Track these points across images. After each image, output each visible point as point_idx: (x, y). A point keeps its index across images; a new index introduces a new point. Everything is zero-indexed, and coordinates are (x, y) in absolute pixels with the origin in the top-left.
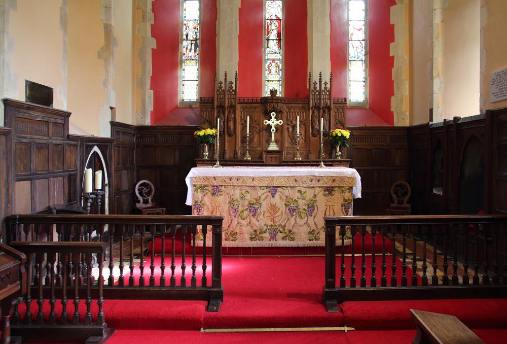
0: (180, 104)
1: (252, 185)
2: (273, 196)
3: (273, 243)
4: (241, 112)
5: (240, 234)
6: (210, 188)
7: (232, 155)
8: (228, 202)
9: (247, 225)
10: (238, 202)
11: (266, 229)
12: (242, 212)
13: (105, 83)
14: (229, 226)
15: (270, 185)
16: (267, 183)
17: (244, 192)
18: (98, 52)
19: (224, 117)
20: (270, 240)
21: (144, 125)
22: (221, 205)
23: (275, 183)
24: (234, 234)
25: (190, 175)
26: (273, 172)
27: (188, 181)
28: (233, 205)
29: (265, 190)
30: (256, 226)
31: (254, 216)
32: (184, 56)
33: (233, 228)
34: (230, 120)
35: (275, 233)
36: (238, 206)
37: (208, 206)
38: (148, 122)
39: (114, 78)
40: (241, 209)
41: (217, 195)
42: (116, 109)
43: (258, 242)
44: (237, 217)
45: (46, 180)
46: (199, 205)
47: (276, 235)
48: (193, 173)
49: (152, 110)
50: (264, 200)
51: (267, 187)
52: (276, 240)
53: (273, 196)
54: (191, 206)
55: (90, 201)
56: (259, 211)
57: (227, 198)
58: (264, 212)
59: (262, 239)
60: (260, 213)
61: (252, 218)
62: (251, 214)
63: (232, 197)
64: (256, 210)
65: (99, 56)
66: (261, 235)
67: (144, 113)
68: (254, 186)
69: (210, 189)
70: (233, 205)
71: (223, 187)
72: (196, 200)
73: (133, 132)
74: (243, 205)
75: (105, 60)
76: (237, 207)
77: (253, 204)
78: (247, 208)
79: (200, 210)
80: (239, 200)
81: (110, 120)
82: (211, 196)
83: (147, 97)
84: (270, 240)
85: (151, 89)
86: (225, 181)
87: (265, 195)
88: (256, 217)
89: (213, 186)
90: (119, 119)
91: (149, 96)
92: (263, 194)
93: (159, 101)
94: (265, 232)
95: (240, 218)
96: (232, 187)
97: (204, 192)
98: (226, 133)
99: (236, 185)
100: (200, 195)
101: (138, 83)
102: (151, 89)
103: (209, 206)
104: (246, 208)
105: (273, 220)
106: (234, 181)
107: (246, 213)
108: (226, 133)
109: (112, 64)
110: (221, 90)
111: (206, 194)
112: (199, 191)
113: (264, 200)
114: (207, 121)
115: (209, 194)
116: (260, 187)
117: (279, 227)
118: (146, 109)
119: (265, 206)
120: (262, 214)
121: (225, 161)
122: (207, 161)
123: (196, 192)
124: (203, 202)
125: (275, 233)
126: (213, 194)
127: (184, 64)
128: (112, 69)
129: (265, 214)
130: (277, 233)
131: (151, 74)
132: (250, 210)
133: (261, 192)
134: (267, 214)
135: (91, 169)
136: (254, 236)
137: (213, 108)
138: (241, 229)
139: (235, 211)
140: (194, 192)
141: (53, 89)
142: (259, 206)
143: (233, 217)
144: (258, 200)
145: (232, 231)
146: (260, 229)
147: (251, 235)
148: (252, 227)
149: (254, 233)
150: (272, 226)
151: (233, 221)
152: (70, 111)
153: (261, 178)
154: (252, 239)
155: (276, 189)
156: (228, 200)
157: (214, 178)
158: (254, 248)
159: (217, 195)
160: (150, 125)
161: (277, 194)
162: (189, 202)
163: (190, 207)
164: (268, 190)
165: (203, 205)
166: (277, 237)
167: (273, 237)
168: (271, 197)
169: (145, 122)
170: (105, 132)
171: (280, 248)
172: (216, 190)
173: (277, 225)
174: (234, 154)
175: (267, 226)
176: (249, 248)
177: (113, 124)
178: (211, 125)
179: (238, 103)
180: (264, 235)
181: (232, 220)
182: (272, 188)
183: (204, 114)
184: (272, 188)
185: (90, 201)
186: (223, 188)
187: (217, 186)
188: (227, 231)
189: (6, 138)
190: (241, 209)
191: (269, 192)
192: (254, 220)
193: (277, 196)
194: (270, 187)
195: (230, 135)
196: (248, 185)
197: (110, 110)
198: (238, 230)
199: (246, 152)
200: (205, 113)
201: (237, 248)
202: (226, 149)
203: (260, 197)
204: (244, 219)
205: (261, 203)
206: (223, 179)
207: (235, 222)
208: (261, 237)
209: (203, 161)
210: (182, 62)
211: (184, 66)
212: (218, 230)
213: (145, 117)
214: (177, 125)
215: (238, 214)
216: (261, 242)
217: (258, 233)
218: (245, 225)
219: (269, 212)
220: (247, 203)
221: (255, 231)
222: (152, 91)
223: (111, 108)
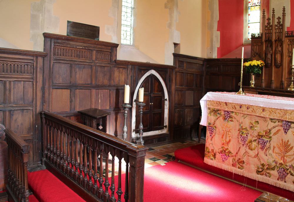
0: (245, 42)
1: (262, 115)
2: (286, 132)
3: (281, 184)
4: (289, 45)
5: (247, 164)
6: (223, 113)
7: (278, 85)
8: (237, 129)
9: (255, 157)
10: (247, 130)
11: (275, 167)
12: (251, 142)
13: (170, 26)
14: (237, 153)
15: (282, 119)
16: (278, 115)
17: (254, 122)
18: (165, 4)
19: (272, 49)
20: (278, 179)
21: (212, 58)
22: (231, 131)
23: (288, 118)
24: (241, 162)
25: (205, 98)
26: (286, 105)
27: (203, 102)
28: (242, 133)
29: (277, 123)
30: (264, 160)
31: (262, 148)
32: (250, 4)
33: (240, 156)
34: (277, 53)
35: (284, 173)
36: (247, 135)
37: (219, 130)
38: (215, 56)
39: (178, 22)
40: (249, 138)
41: (228, 121)
42: (181, 44)
43: (264, 177)
44: (245, 146)
45: (90, 91)
46: (212, 127)
47: (286, 176)
48: (208, 96)
49: (219, 46)
50: (275, 134)
51: (279, 121)
52: (285, 182)
53: (286, 132)
54: (206, 126)
55: (127, 109)
56: (268, 144)
57: (237, 125)
58: (274, 147)
59: (270, 176)
60: (269, 147)
61: (260, 150)
62: (260, 146)
63: (241, 125)
64: (265, 143)
65: (166, 7)
66: (268, 171)
67: (212, 48)
68: (264, 118)
69: (222, 114)
70: (242, 133)
71: (234, 113)
72: (209, 122)
73: (201, 63)
74: (252, 136)
75: (170, 9)
76: (245, 136)
77: (262, 136)
78: (256, 138)
79: (212, 131)
80: (248, 129)
81: (173, 52)
82: (223, 120)
83: (214, 37)
84: (278, 179)
85: (218, 30)
86: (235, 108)
87: (277, 128)
88: (264, 150)
89: (225, 111)
90: (183, 52)
91: (216, 36)
92: (274, 127)
93: (224, 39)
94: (273, 169)
95: (248, 147)
96: (242, 115)
97: (217, 116)
98: (273, 64)
99: (246, 113)
100: (213, 118)
101: (206, 26)
102: (218, 30)
103: (221, 130)
104: (254, 139)
105: (283, 157)
106: (244, 108)
107: (254, 144)
108: (273, 64)
109: (175, 12)
110: (269, 26)
111: (219, 118)
112: (212, 113)
113: (275, 134)
114: (257, 54)
115: (221, 118)
116: (271, 119)
117: (290, 167)
118: (213, 46)
119: (275, 141)
120: (272, 148)
121: (261, 89)
122: (252, 88)
123: (209, 115)
124: (215, 125)
125: (284, 173)
126: (225, 119)
127: (249, 10)
128: (175, 14)
129: (275, 150)
130: (288, 174)
131: (218, 19)
132: (259, 142)
133: (271, 125)
134: (277, 150)
135: (143, 88)
136: (260, 170)
137: (262, 43)
138: (248, 159)
139: (244, 140)
140: (209, 114)
141: (99, 27)
142: (269, 140)
143: (241, 145)
144: (268, 132)
145: (240, 159)
146: (268, 165)
147: (258, 168)
148: (259, 160)
149: (261, 167)
150: (281, 164)
151: (240, 149)
152: (118, 44)
153: (273, 110)
154: (258, 172)
155: (289, 124)
156: (238, 127)
157: (226, 103)
158: (259, 182)
159: (228, 121)
160: (216, 58)
161: (290, 130)
162: (203, 122)
163: (204, 128)
164: (280, 124)
165: (216, 128)
166: (286, 178)
167: (282, 177)
168: (283, 132)
169: (212, 55)
170: (169, 61)
171: (289, 191)
172: (228, 116)
173: (288, 164)
174: (281, 84)
175: (276, 163)
176: (255, 181)
177: (176, 55)
178: (260, 57)
179: (286, 37)
180: (272, 172)
181: (240, 148)
182: (284, 122)
183: (254, 48)
184: (284, 122)
185: (127, 109)
186: (233, 115)
187: (228, 112)
188: (234, 157)
189: (44, 60)
190: (249, 138)
191: (281, 126)
192: (262, 153)
193: (290, 132)
194: (282, 121)
195: (277, 67)
196: (257, 115)
197: (174, 45)
198: (245, 159)
199: (291, 83)
200: (255, 47)
201: (243, 177)
202: (273, 79)
203: (270, 131)
204: (251, 150)
205: (270, 137)
206: (234, 106)
207: (243, 150)
208: (268, 173)
209: (249, 88)
210: (247, 8)
211: (249, 12)
212: (134, 163)
213: (213, 52)
214: (234, 57)
215: (246, 143)
216: (268, 178)
217: (265, 167)
218: (253, 156)
219: (279, 148)
220: (256, 134)
221: (263, 165)
222: (219, 33)
223: (176, 44)
